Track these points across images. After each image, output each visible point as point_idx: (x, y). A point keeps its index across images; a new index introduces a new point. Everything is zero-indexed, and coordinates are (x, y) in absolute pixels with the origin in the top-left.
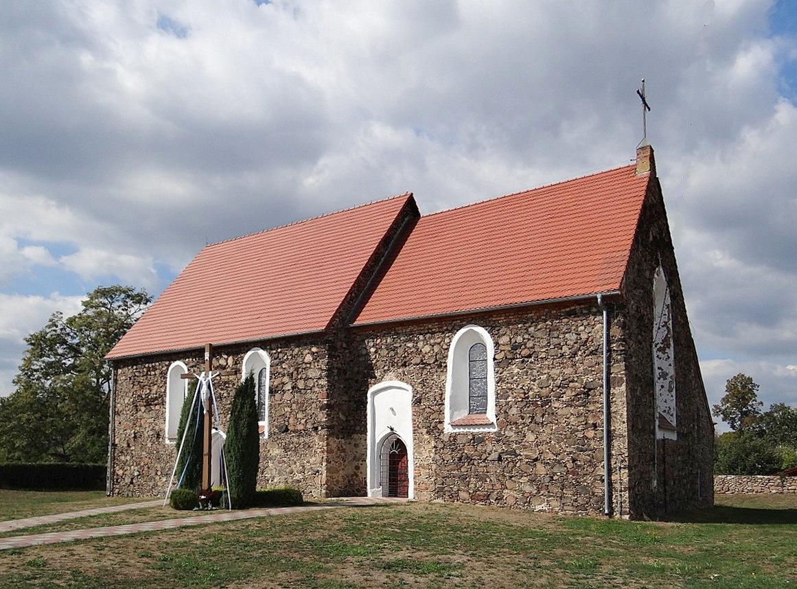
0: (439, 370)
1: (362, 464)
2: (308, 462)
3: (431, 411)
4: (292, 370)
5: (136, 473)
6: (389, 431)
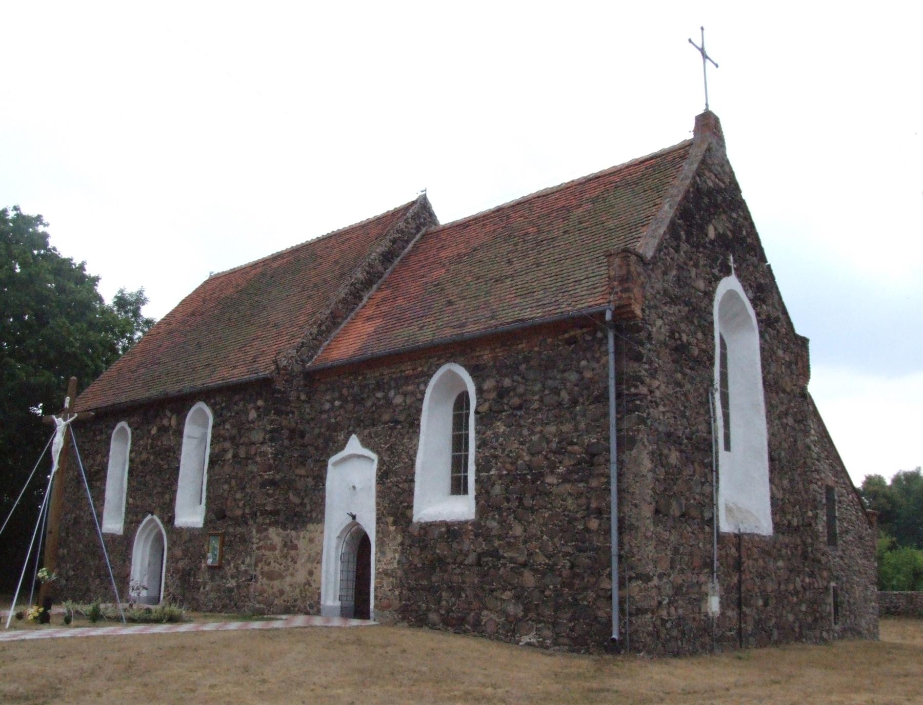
0: (411, 431)
2: (243, 563)
4: (234, 432)
5: (71, 573)
6: (350, 519)
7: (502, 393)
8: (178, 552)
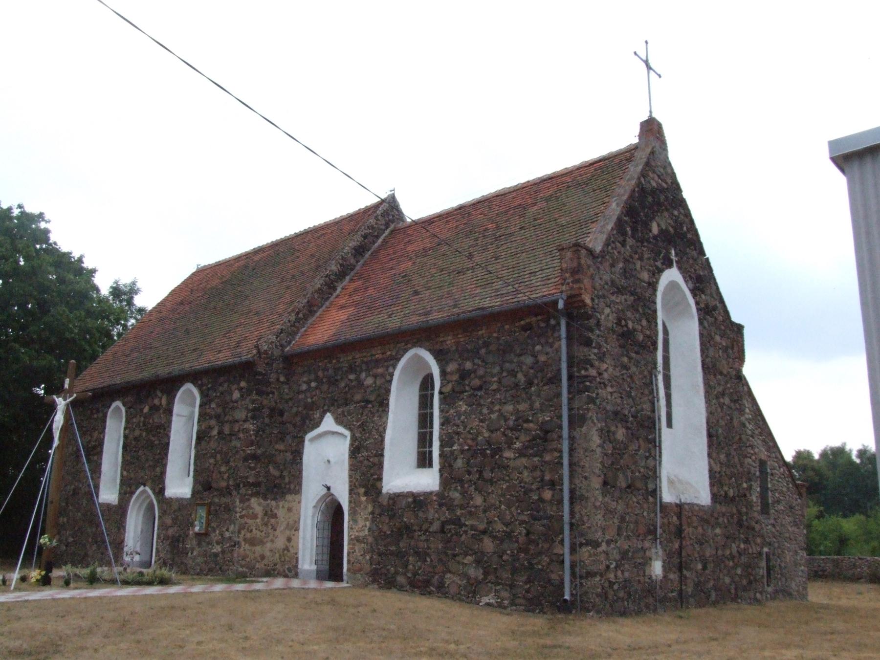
1: (294, 535)
2: (227, 530)
3: (370, 464)
4: (219, 410)
5: (71, 539)
6: (325, 491)
7: (464, 375)
8: (168, 521)
